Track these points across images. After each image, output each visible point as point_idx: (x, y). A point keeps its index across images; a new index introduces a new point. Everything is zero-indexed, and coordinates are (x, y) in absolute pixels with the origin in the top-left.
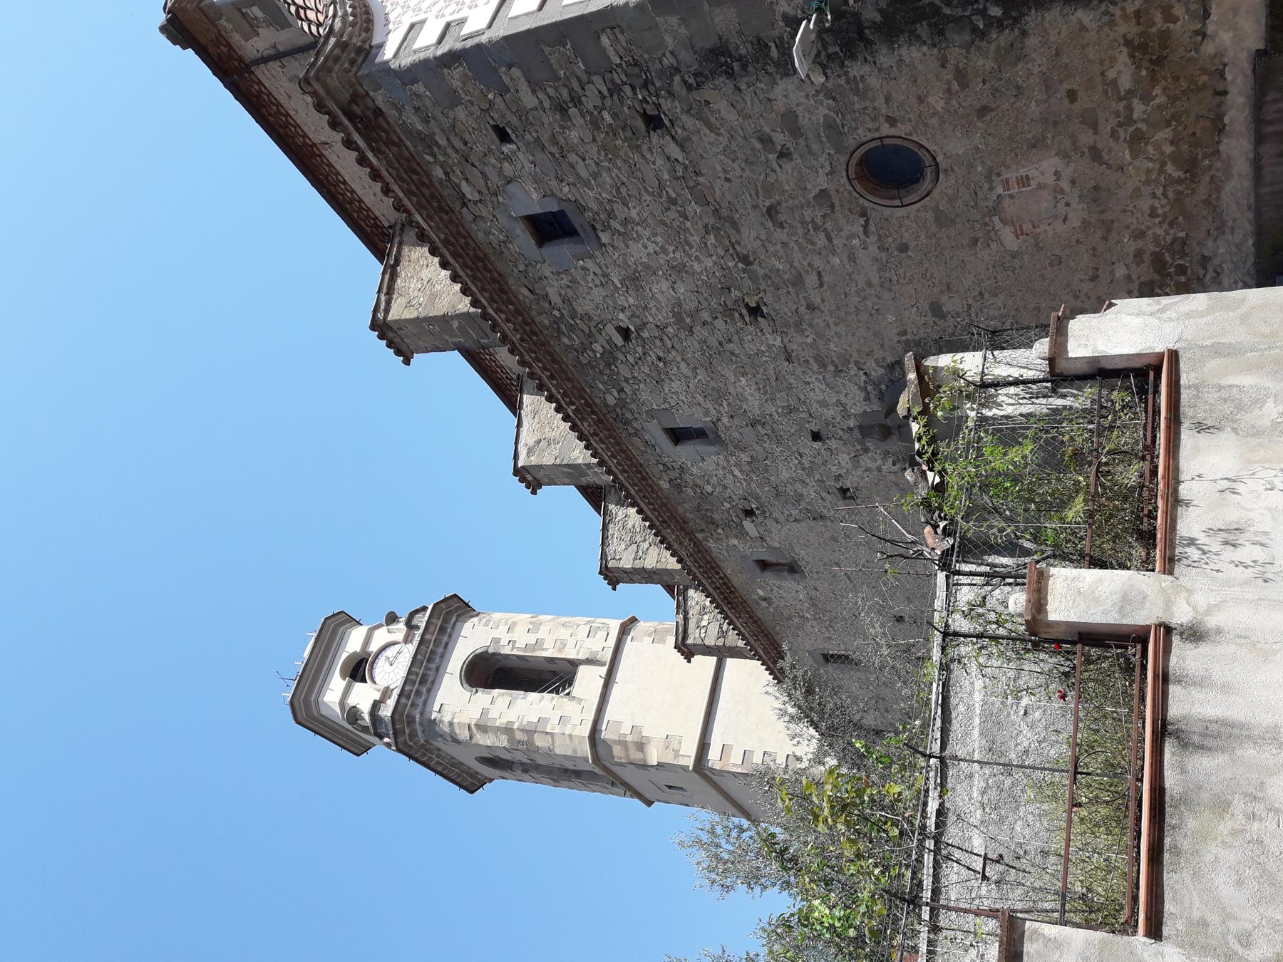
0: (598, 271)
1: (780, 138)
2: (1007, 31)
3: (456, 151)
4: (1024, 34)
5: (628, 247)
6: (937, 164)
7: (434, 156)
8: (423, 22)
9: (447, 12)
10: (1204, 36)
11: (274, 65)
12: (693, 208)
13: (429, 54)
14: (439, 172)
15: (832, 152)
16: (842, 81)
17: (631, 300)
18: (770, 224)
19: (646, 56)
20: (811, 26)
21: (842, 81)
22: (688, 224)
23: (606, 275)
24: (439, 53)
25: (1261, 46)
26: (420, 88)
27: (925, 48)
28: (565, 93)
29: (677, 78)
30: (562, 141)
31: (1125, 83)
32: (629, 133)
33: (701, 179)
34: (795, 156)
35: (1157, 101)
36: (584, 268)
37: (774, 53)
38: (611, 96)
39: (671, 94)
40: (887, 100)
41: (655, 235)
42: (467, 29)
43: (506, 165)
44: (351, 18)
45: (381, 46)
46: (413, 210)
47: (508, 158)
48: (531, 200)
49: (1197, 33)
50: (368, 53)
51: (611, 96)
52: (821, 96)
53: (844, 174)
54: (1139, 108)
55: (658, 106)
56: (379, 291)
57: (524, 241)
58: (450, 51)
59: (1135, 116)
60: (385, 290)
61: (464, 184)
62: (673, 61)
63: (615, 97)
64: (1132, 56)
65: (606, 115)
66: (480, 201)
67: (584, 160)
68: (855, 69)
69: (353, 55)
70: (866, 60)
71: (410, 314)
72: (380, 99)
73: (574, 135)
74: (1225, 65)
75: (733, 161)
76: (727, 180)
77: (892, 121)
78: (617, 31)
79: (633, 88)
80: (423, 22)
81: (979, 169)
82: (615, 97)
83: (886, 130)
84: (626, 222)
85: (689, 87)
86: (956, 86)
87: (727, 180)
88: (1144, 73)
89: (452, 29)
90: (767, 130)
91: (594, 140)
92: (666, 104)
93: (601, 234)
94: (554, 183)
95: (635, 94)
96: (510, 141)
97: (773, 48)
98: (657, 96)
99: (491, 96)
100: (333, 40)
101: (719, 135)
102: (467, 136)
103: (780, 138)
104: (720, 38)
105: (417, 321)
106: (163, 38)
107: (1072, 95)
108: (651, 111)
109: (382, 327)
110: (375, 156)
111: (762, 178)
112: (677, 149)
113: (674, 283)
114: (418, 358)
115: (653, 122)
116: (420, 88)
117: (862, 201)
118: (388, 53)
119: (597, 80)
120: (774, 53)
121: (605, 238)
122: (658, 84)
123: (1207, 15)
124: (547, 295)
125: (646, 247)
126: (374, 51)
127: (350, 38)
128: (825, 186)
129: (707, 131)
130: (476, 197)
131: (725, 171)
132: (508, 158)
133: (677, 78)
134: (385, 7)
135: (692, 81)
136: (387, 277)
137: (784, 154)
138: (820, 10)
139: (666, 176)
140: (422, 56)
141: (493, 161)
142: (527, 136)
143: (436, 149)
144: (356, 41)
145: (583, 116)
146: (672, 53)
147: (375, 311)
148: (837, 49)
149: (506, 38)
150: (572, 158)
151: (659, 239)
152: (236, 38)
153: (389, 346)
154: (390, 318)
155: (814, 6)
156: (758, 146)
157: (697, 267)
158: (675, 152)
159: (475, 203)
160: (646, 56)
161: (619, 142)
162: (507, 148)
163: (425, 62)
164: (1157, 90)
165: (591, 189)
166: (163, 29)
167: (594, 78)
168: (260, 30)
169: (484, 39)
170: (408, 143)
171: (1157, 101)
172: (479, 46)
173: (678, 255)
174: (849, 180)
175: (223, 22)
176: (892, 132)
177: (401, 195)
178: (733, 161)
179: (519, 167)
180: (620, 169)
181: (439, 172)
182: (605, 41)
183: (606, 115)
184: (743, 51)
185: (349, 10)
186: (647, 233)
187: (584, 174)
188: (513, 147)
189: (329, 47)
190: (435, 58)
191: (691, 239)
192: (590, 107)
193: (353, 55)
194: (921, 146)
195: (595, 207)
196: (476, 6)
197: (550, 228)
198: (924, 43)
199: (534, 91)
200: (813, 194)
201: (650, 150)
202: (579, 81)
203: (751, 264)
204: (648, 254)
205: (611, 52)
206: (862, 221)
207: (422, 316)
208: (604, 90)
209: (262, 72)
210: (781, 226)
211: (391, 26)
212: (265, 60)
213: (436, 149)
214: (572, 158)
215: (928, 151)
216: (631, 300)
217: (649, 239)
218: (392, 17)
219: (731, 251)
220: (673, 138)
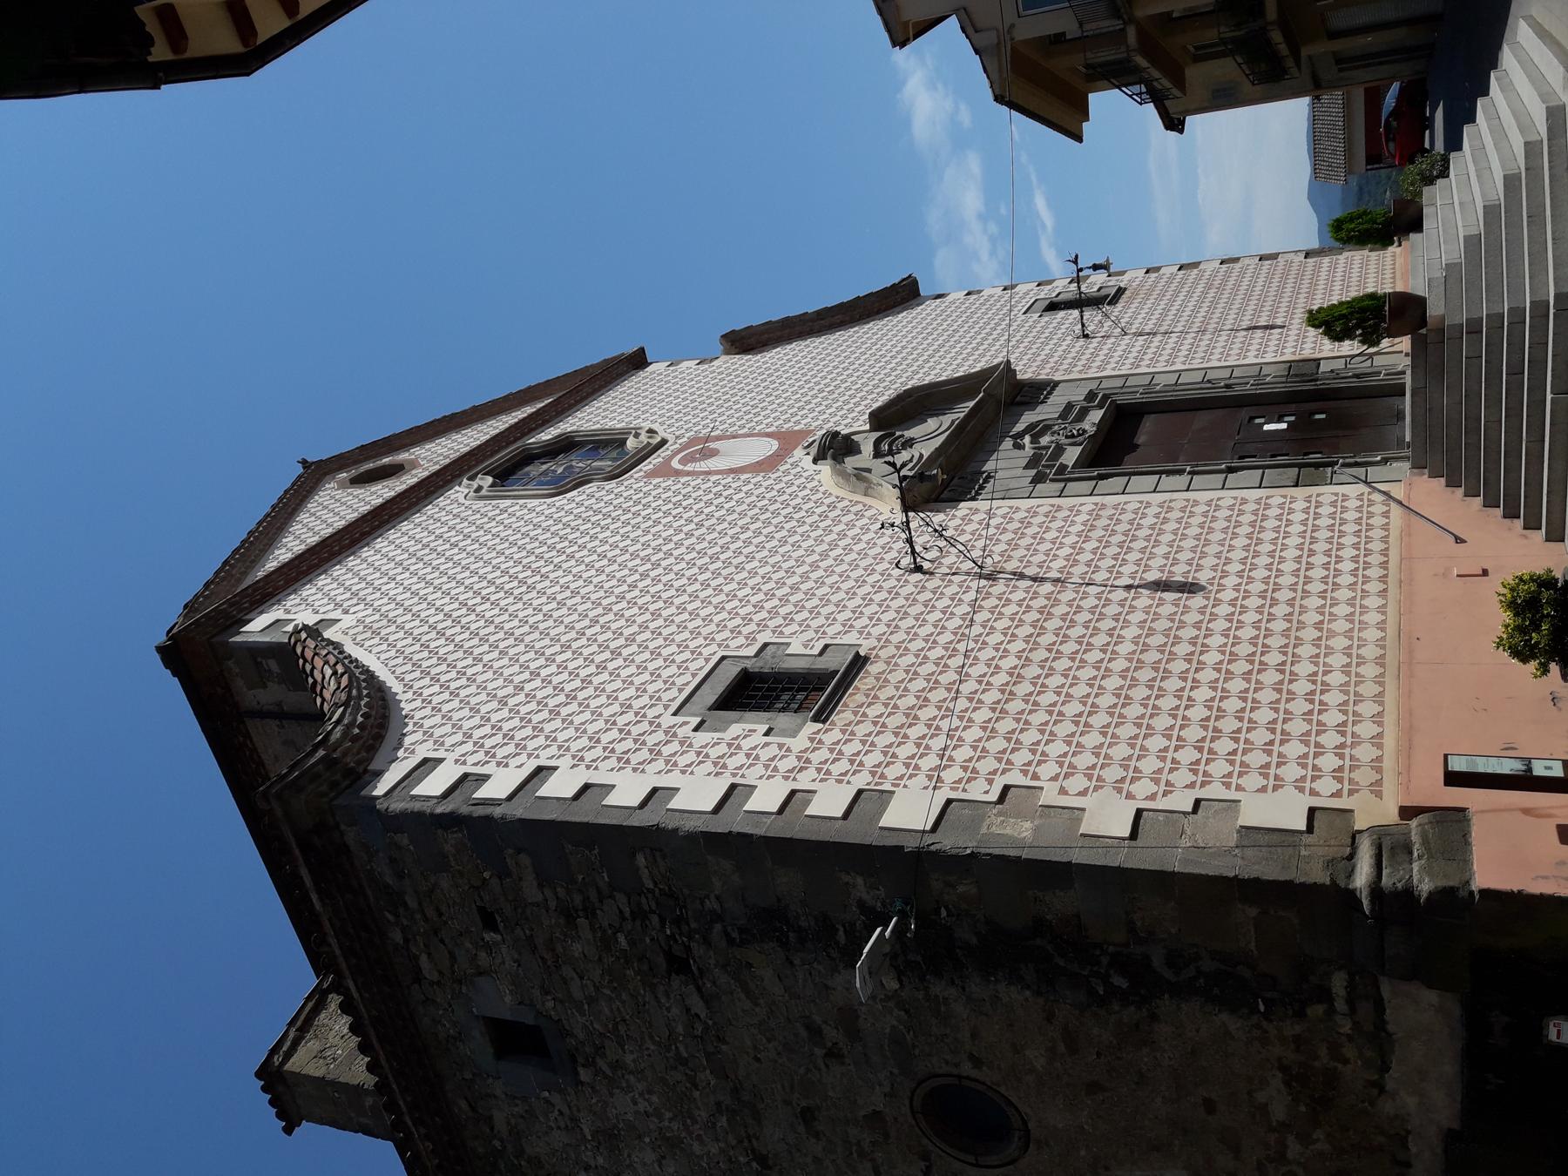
0: (566, 1111)
1: (832, 1034)
2: (1132, 1008)
3: (426, 920)
4: (1154, 1017)
5: (612, 1095)
6: (1028, 1131)
7: (397, 916)
8: (441, 761)
9: (471, 760)
10: (1382, 1090)
11: (273, 724)
12: (706, 1076)
13: (427, 807)
14: (397, 937)
15: (896, 1071)
16: (920, 995)
17: (600, 1160)
18: (801, 1129)
19: (686, 891)
20: (887, 934)
21: (920, 995)
22: (697, 1094)
23: (574, 1119)
24: (439, 810)
25: (1456, 1125)
26: (404, 840)
27: (1028, 993)
28: (578, 899)
29: (718, 927)
30: (560, 950)
31: (1279, 1112)
32: (645, 967)
33: (724, 1048)
34: (847, 1061)
35: (1318, 1146)
36: (547, 1101)
37: (841, 937)
38: (634, 920)
39: (707, 941)
40: (974, 1036)
41: (650, 1092)
42: (483, 793)
43: (483, 954)
44: (357, 731)
45: (378, 774)
46: (347, 973)
47: (488, 947)
48: (500, 1000)
49: (1373, 1084)
50: (359, 777)
51: (634, 920)
52: (891, 1004)
53: (907, 1102)
54: (1294, 1149)
55: (688, 949)
56: (291, 1024)
57: (478, 1047)
58: (452, 813)
59: (1290, 1155)
60: (299, 1023)
61: (424, 958)
62: (716, 906)
63: (638, 923)
64: (1287, 1084)
65: (621, 938)
66: (438, 983)
67: (582, 978)
68: (938, 988)
69: (338, 777)
70: (953, 983)
71: (316, 1070)
72: (351, 836)
73: (577, 948)
74: (1409, 1132)
75: (769, 1041)
76: (758, 1060)
77: (977, 1062)
78: (658, 854)
79: (662, 920)
80: (441, 761)
81: (1083, 1153)
82: (638, 923)
83: (967, 1069)
84: (617, 1065)
85: (731, 942)
86: (1062, 1048)
87: (758, 1060)
88: (1303, 1109)
89: (466, 784)
90: (818, 1019)
91: (600, 959)
92: (698, 950)
93: (581, 1071)
94: (537, 993)
95: (663, 926)
96: (496, 930)
97: (841, 932)
98: (690, 938)
99: (486, 875)
100: (321, 753)
101: (757, 1005)
102: (444, 909)
103: (832, 1034)
104: (779, 900)
105: (320, 1081)
106: (157, 657)
107: (1209, 1106)
108: (678, 951)
109: (273, 1077)
110: (321, 900)
111: (802, 1071)
112: (701, 1003)
113: (664, 1157)
114: (306, 1129)
115: (679, 965)
116: (404, 840)
117: (925, 1141)
118: (381, 789)
119: (621, 898)
120: (841, 937)
121: (584, 1074)
122: (694, 925)
123: (1385, 1068)
124: (491, 1118)
125: (635, 1103)
126: (367, 777)
127: (345, 754)
128: (880, 1107)
129: (743, 996)
130: (435, 977)
131: (755, 1048)
132: (488, 947)
133: (718, 927)
134: (406, 725)
135: (735, 935)
136: (310, 1004)
137: (833, 1054)
138: (903, 916)
139: (680, 1029)
140: (417, 806)
141: (468, 945)
142: (518, 931)
143: (401, 910)
144: (350, 761)
145: (593, 929)
146: (717, 898)
147: (274, 1051)
148: (919, 958)
149: (522, 821)
150: (567, 971)
151: (655, 1099)
152: (239, 684)
153: (271, 1103)
154: (286, 1067)
155: (898, 905)
156: (804, 1033)
157: (697, 1148)
158: (698, 1006)
159: (432, 984)
160: (686, 891)
161: (630, 973)
162: (489, 936)
163: (419, 816)
164: (1318, 1134)
165: (582, 1014)
166: (160, 649)
167: (618, 895)
168: (270, 684)
169: (497, 812)
170: (369, 892)
171: (1318, 1146)
172: (488, 819)
173: (675, 1125)
174: (913, 1112)
175: (230, 663)
176: (974, 1073)
177: (338, 952)
178: (769, 1041)
179: (498, 961)
180: (623, 1002)
181: (397, 937)
182: (641, 860)
183: (621, 938)
184: (804, 924)
185: (360, 719)
186: (640, 1086)
187: (577, 994)
188: (499, 937)
189: (313, 761)
190: (432, 815)
191: (696, 1113)
192: (605, 924)
193: (338, 777)
194: (1010, 1103)
195: (581, 1036)
196: (506, 765)
197: (516, 1040)
198: (1028, 987)
199: (541, 886)
200: (862, 1113)
201: (668, 997)
202: (599, 892)
203: (770, 1168)
204: (637, 1112)
205: (645, 873)
206: (923, 1164)
207: (330, 1077)
208: (627, 911)
209: (255, 728)
210: (817, 1135)
211: (400, 753)
212: (262, 714)
213: (401, 910)
214: (567, 971)
215: (1017, 1109)
216: (600, 1160)
217: (641, 1094)
218: (407, 741)
219: (746, 1144)
220: (699, 989)
